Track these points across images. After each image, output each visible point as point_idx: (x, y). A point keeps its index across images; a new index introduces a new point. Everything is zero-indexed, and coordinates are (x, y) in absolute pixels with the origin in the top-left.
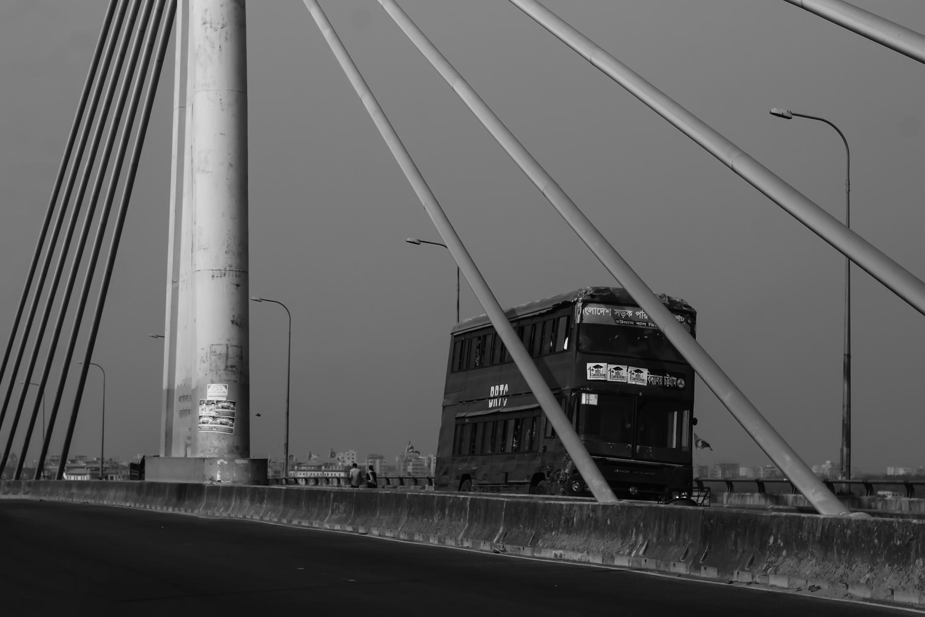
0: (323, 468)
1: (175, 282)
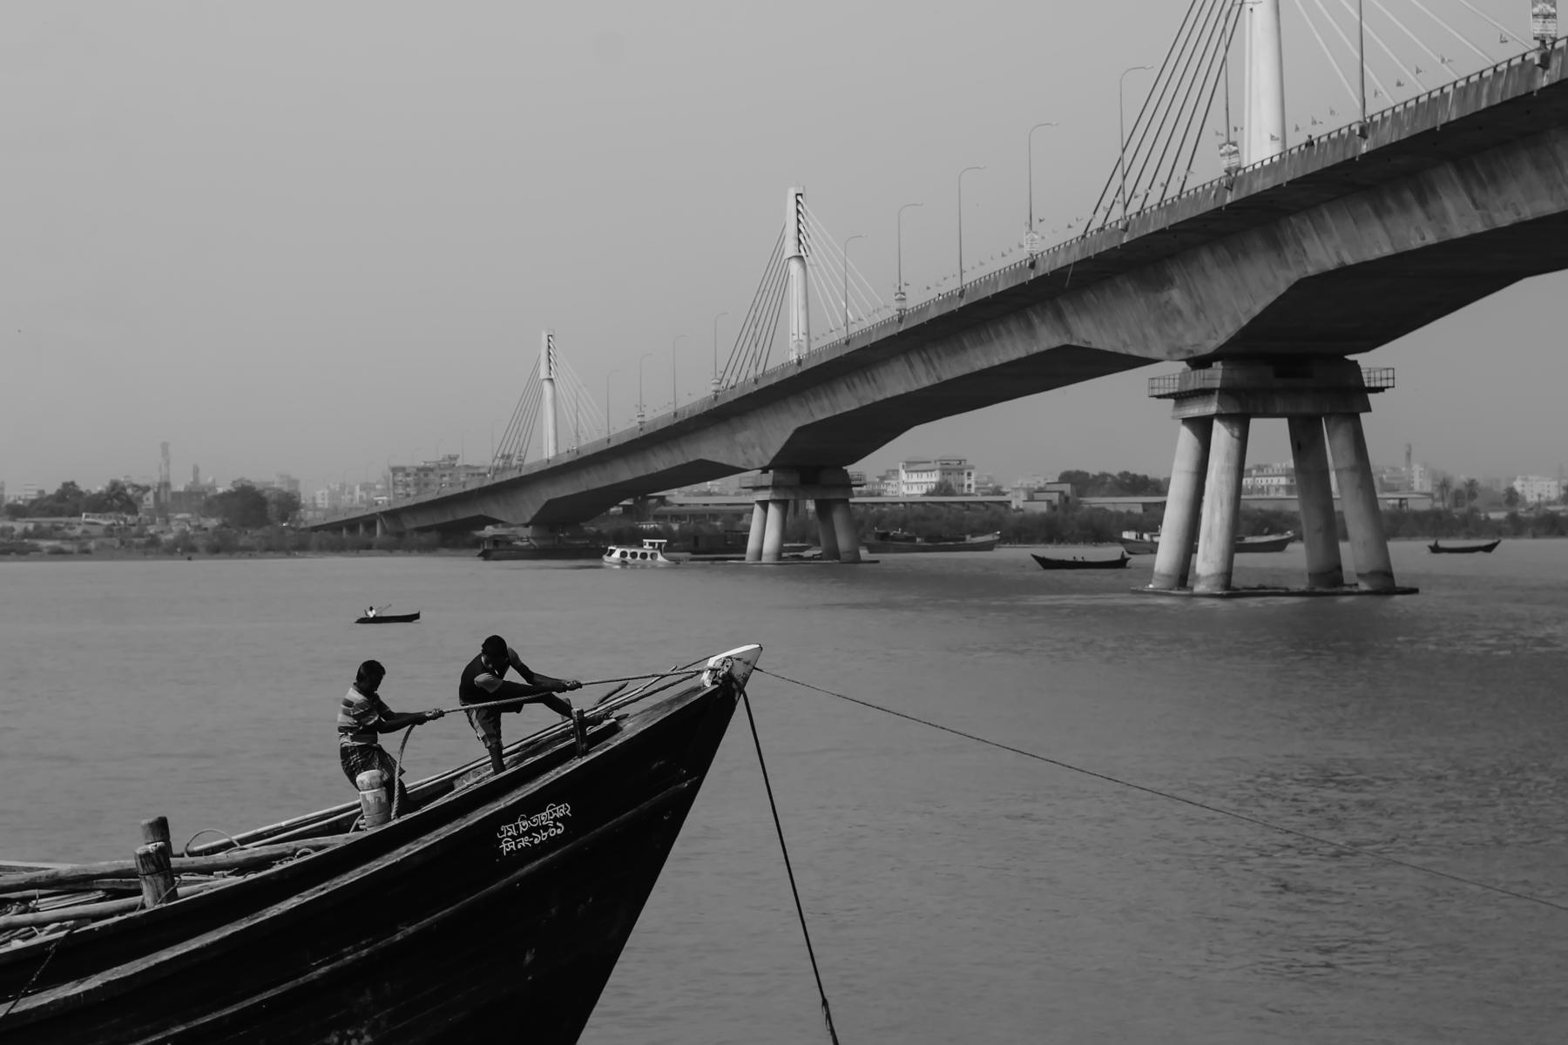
0: (1254, 472)
1: (534, 735)
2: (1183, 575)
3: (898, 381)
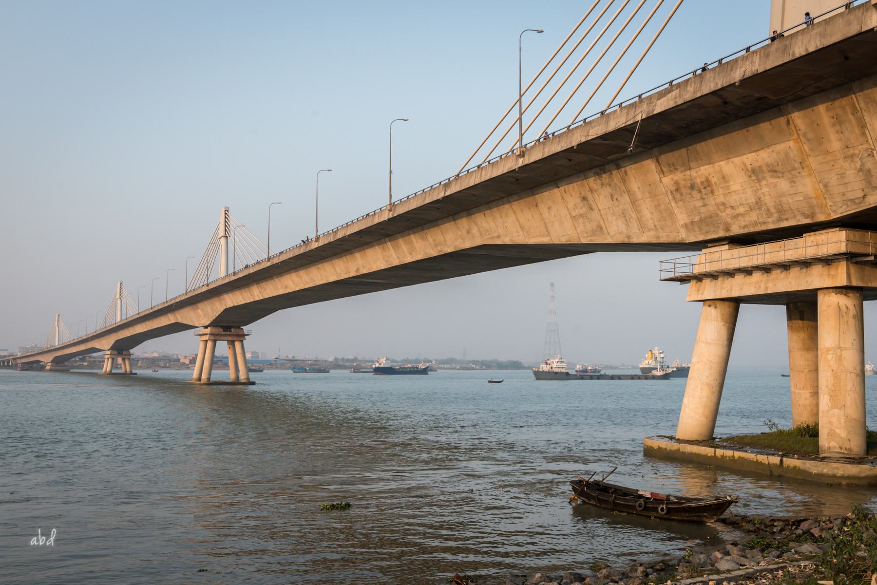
2: (200, 379)
3: (140, 329)
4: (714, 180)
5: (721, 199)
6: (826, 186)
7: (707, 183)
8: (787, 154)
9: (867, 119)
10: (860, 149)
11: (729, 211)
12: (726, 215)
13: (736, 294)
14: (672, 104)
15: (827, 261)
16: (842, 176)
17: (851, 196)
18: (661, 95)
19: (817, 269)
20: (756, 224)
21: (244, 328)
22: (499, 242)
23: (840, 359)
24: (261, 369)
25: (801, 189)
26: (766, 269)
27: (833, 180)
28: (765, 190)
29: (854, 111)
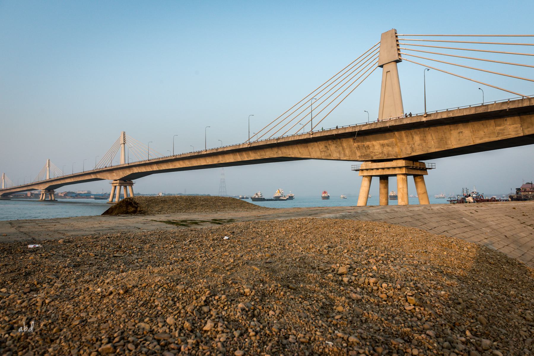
4: (370, 146)
5: (371, 150)
6: (401, 150)
7: (368, 146)
8: (392, 142)
9: (414, 136)
10: (411, 143)
11: (373, 154)
12: (372, 155)
13: (370, 174)
14: (367, 128)
15: (400, 168)
16: (406, 148)
17: (407, 153)
18: (364, 125)
19: (397, 169)
20: (381, 157)
21: (133, 181)
22: (289, 156)
23: (403, 190)
24: (106, 198)
25: (395, 150)
26: (383, 169)
27: (404, 149)
28: (385, 149)
29: (411, 134)
